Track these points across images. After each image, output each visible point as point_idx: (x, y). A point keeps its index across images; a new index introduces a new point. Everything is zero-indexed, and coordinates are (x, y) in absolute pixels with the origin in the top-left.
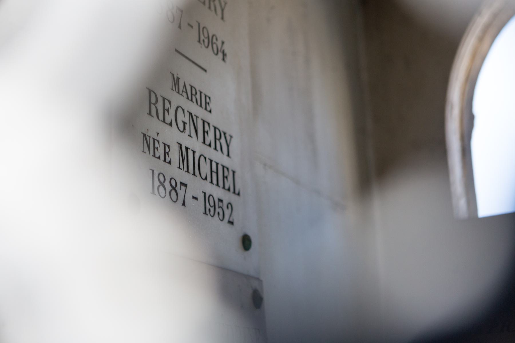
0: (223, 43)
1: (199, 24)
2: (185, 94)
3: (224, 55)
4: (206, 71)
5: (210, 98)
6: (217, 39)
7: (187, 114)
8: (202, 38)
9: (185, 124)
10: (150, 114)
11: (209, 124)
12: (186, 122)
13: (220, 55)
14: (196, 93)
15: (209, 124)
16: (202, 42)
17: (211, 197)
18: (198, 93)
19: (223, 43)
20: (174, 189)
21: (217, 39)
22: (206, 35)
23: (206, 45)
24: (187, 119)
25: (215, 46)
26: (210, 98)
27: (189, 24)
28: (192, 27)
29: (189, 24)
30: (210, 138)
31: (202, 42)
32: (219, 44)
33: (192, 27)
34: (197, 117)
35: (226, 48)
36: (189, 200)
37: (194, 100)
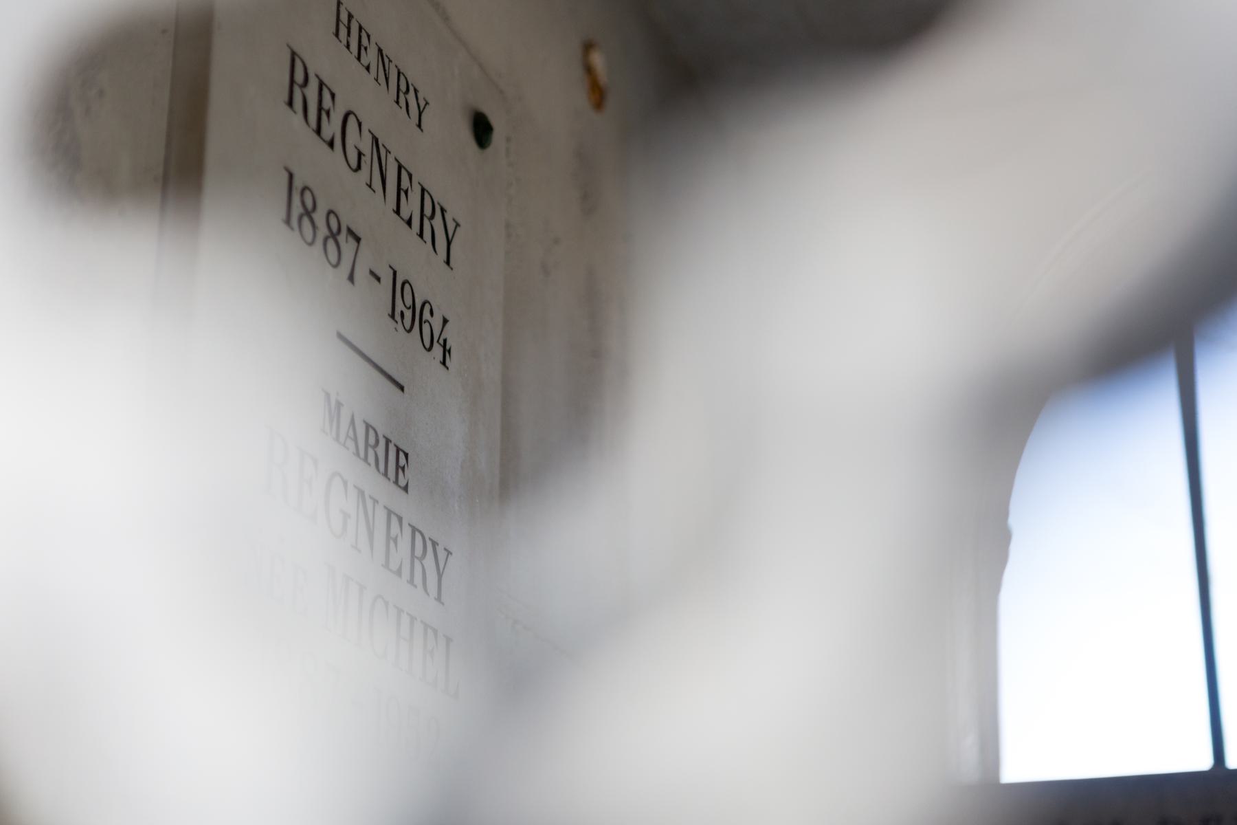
0: (445, 321)
1: (395, 273)
2: (350, 444)
3: (446, 351)
4: (402, 388)
5: (406, 455)
6: (432, 313)
7: (367, 139)
8: (400, 306)
9: (360, 154)
10: (290, 103)
11: (410, 176)
12: (363, 151)
13: (438, 350)
14: (377, 441)
15: (410, 176)
16: (398, 317)
17: (407, 286)
18: (382, 442)
19: (445, 321)
20: (334, 236)
21: (432, 313)
22: (409, 302)
23: (408, 326)
24: (366, 146)
25: (426, 328)
26: (406, 455)
27: (372, 273)
28: (378, 279)
29: (372, 273)
30: (411, 206)
31: (398, 317)
32: (437, 323)
33: (378, 279)
34: (388, 151)
35: (451, 334)
36: (361, 274)
37: (371, 459)
